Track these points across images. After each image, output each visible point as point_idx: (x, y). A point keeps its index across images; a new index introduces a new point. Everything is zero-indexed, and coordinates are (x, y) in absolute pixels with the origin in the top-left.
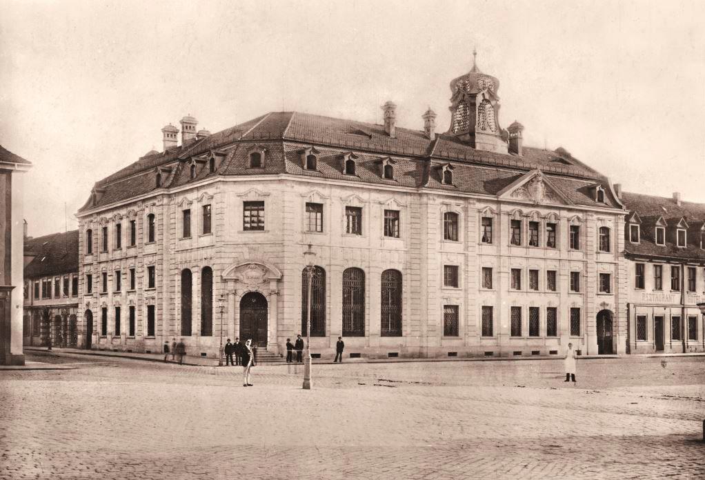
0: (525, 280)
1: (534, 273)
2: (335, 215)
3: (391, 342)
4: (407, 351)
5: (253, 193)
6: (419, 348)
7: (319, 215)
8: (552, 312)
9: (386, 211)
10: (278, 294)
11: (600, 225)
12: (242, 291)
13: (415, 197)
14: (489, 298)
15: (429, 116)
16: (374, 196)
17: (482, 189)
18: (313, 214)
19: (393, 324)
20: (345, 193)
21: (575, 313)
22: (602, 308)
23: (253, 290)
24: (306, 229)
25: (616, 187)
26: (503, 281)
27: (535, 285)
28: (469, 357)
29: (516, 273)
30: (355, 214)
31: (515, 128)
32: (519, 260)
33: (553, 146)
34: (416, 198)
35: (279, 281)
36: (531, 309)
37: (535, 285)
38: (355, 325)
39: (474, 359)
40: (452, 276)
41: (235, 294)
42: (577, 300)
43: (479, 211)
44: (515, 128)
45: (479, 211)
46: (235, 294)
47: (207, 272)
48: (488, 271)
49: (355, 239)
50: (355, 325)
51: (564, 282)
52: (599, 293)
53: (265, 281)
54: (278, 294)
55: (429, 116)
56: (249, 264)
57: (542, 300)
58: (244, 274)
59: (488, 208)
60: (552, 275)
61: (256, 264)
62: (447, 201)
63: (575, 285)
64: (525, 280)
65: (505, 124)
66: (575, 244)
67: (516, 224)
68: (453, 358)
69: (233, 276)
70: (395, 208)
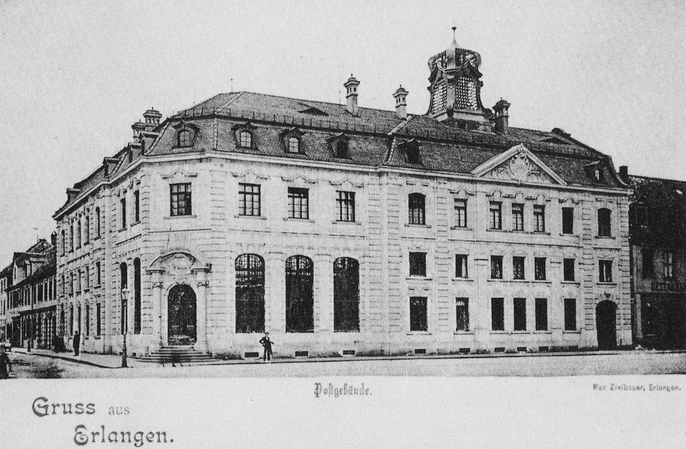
0: (508, 269)
1: (519, 262)
2: (275, 197)
3: (346, 339)
4: (366, 349)
5: (179, 174)
6: (380, 345)
7: (304, 201)
8: (541, 305)
9: (171, 186)
10: (206, 285)
11: (600, 205)
12: (169, 283)
13: (374, 177)
14: (462, 288)
15: (401, 94)
16: (327, 175)
17: (327, 156)
18: (297, 200)
19: (347, 317)
20: (338, 177)
21: (570, 305)
22: (605, 298)
23: (181, 282)
24: (490, 225)
25: (624, 169)
26: (480, 270)
27: (519, 274)
28: (441, 354)
29: (497, 261)
30: (251, 192)
31: (502, 106)
32: (500, 246)
33: (548, 128)
34: (375, 177)
35: (208, 270)
36: (537, 300)
37: (519, 274)
38: (300, 318)
39: (447, 356)
40: (418, 263)
41: (161, 287)
42: (540, 290)
43: (561, 201)
44: (502, 106)
45: (561, 201)
46: (161, 287)
47: (137, 262)
48: (461, 259)
49: (182, 222)
50: (300, 318)
51: (555, 273)
52: (455, 278)
53: (192, 271)
54: (206, 285)
55: (401, 94)
56: (176, 253)
57: (531, 291)
58: (170, 264)
59: (462, 189)
60: (540, 263)
61: (183, 253)
62: (412, 180)
63: (569, 274)
64: (508, 269)
65: (489, 102)
66: (568, 227)
67: (496, 207)
68: (421, 356)
69: (157, 267)
70: (349, 189)
